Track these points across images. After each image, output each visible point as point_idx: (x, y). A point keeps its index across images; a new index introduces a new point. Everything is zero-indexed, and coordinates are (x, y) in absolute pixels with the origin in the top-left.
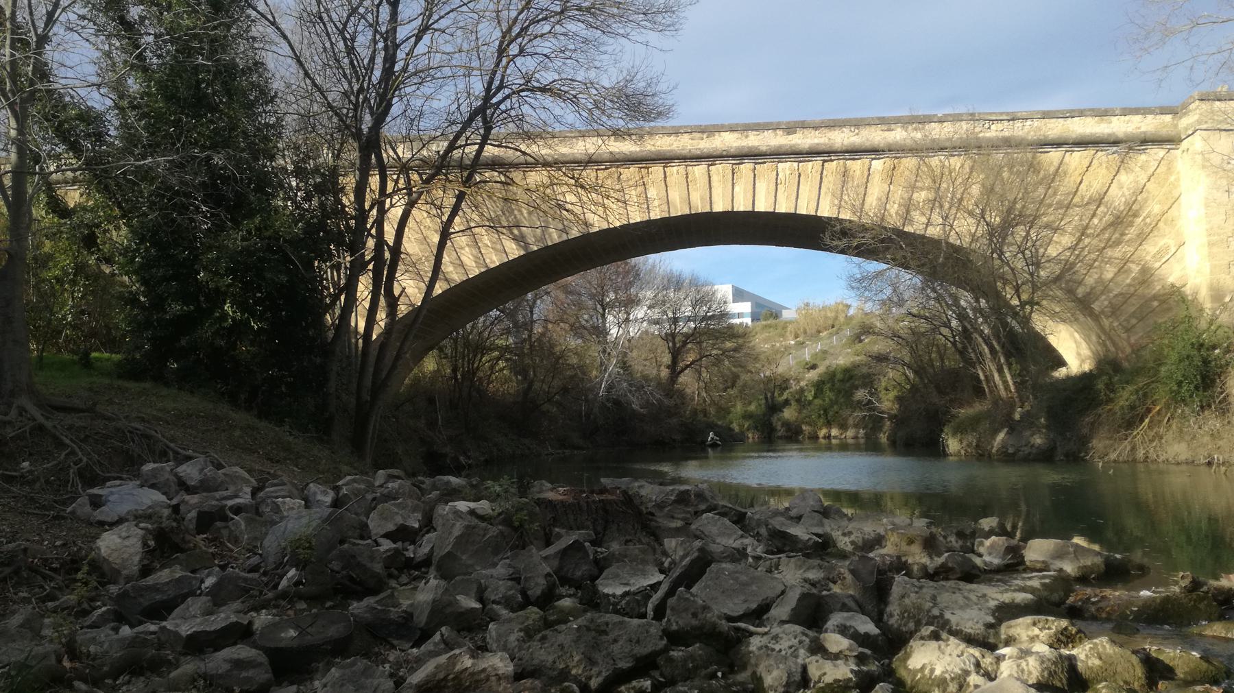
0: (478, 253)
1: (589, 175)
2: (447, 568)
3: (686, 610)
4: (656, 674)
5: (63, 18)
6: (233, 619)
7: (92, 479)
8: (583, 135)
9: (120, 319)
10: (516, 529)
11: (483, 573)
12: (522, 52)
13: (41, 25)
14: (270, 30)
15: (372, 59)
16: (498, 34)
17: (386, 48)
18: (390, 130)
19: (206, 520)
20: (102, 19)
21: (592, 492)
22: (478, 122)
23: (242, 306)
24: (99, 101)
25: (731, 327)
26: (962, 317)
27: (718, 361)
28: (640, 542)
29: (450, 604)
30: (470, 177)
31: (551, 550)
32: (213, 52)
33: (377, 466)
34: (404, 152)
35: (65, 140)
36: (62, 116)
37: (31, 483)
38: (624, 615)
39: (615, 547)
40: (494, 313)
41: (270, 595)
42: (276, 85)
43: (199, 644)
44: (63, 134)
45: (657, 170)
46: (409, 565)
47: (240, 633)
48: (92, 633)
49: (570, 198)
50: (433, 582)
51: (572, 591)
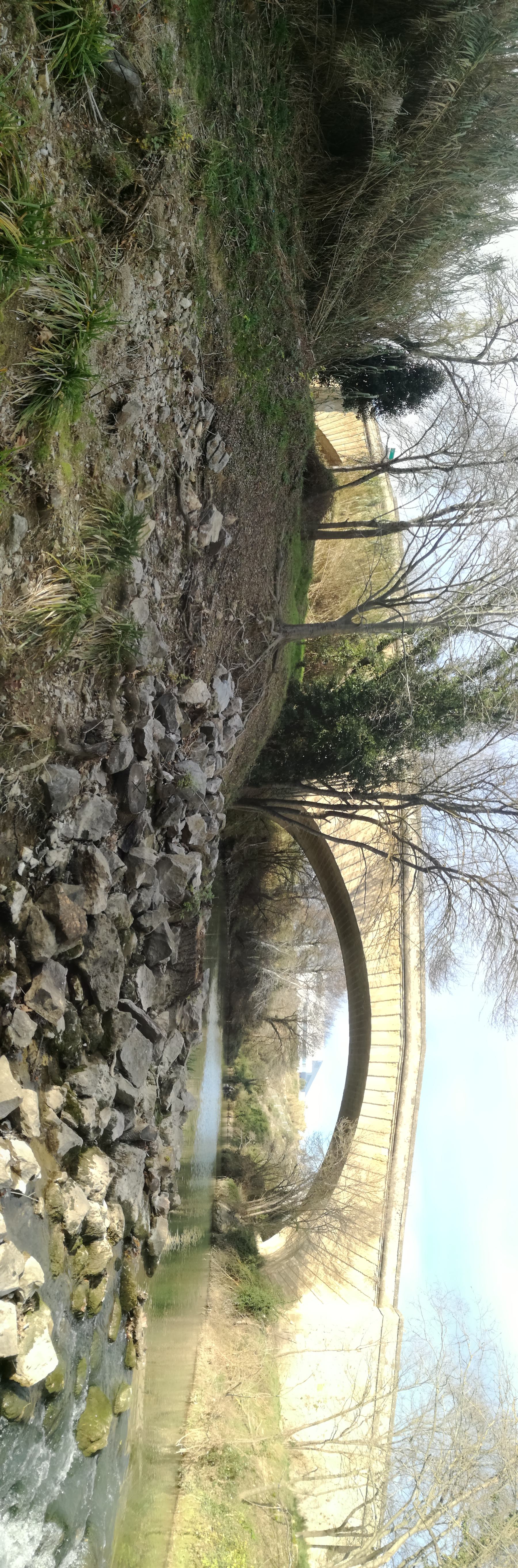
0: (350, 865)
1: (396, 935)
2: (163, 864)
3: (124, 1024)
4: (86, 1004)
5: (488, 638)
6: (149, 751)
7: (235, 675)
8: (421, 931)
9: (322, 680)
10: (182, 904)
11: (158, 885)
12: (473, 890)
13: (484, 628)
14: (483, 743)
15: (468, 800)
16: (484, 875)
17: (473, 806)
18: (424, 810)
19: (208, 732)
20: (488, 658)
21: (201, 962)
22: (430, 864)
23: (325, 738)
24: (442, 660)
25: (298, 1059)
26: (293, 1192)
27: (278, 1050)
28: (168, 995)
29: (140, 869)
30: (395, 859)
31: (167, 927)
32: (470, 715)
33: (228, 813)
34: (411, 819)
35: (420, 645)
36: (434, 643)
37: (237, 645)
38: (123, 983)
39: (166, 978)
40: (314, 874)
41: (160, 767)
42: (451, 748)
43: (138, 736)
44: (424, 643)
45: (398, 980)
46: (168, 840)
47: (140, 753)
48: (152, 683)
49: (383, 925)
50: (154, 858)
51: (142, 942)
